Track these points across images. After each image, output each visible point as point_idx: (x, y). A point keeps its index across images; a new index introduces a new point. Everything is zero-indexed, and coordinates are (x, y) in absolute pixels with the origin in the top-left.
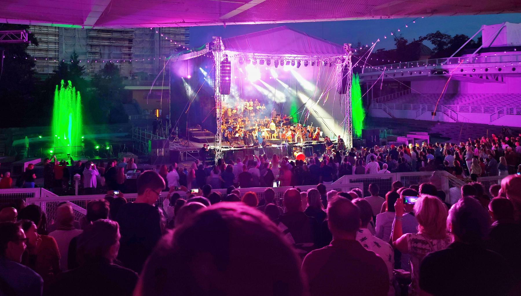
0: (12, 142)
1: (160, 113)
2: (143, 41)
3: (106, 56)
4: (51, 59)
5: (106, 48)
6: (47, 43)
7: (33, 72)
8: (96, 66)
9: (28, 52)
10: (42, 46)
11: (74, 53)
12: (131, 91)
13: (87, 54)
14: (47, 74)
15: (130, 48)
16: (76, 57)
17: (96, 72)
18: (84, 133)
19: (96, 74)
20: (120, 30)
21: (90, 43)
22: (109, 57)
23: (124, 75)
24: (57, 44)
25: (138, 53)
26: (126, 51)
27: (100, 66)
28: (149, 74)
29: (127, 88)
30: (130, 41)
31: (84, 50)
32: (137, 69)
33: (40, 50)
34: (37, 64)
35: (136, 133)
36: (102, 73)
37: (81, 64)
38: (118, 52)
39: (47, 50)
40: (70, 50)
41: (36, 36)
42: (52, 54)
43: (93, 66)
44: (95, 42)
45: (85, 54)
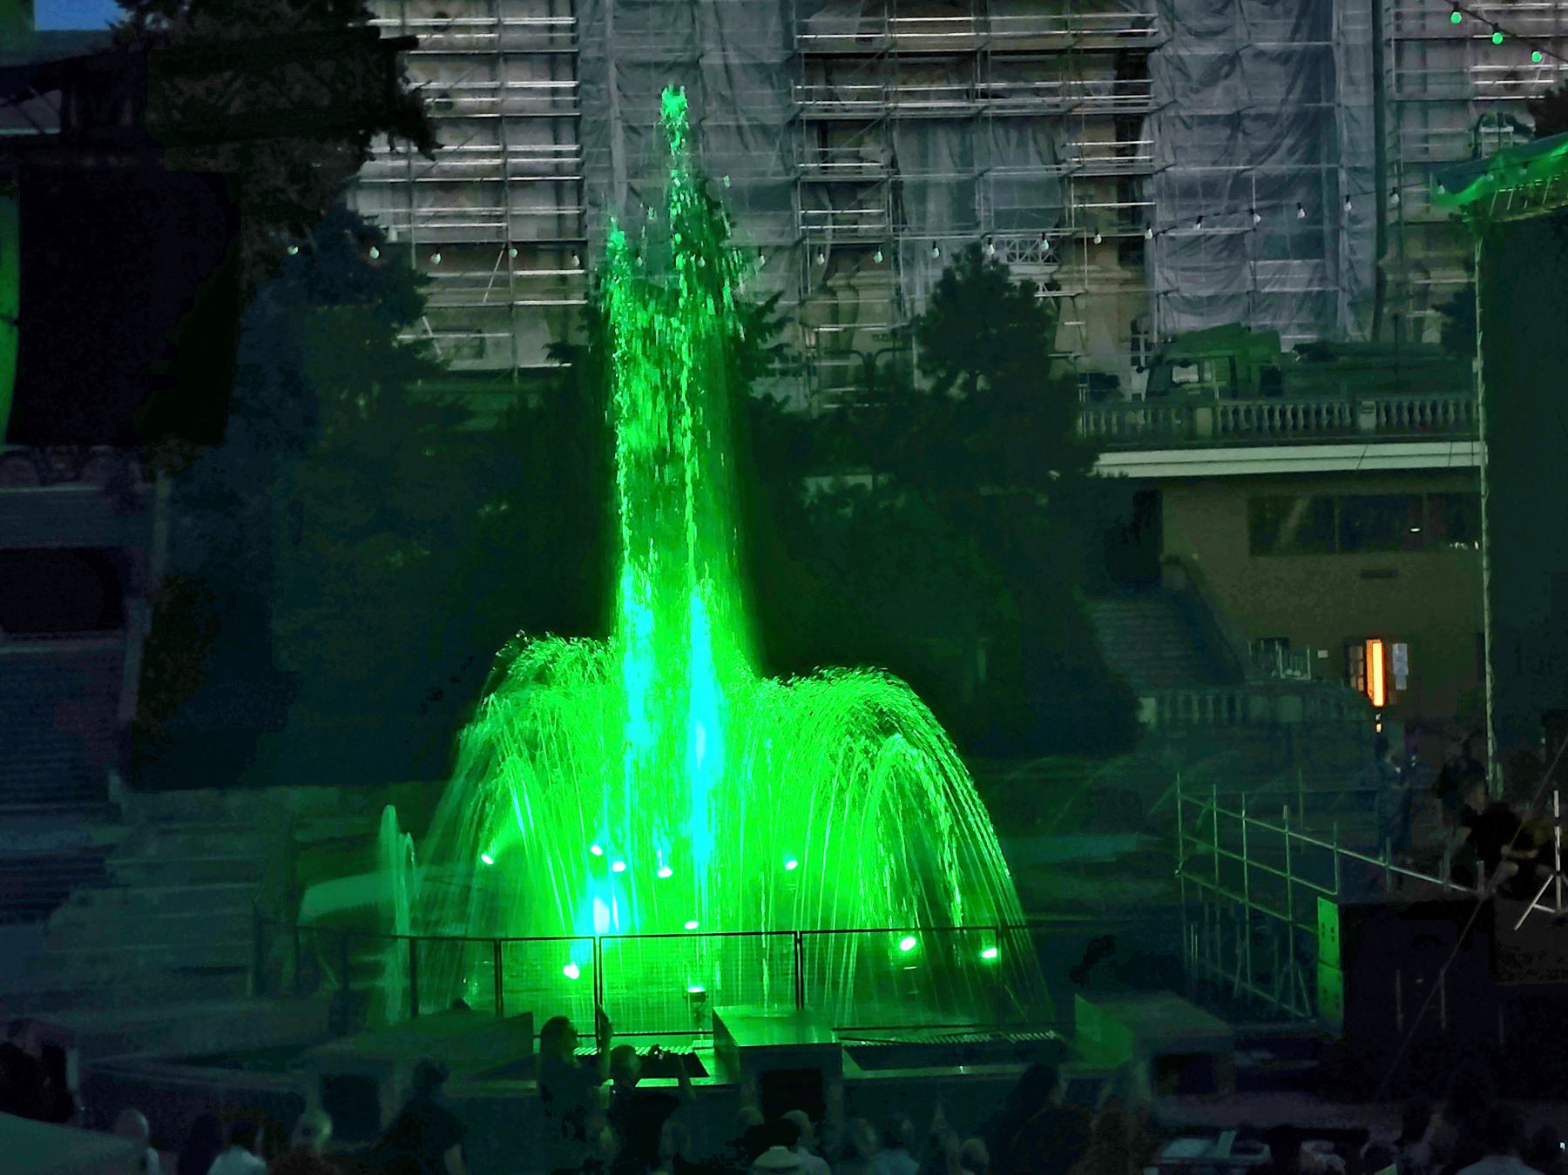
0: (295, 895)
1: (1401, 668)
2: (1233, 60)
5: (944, 144)
6: (494, 126)
7: (414, 362)
8: (865, 298)
9: (365, 206)
10: (464, 154)
12: (1149, 493)
13: (796, 198)
14: (505, 375)
15: (1127, 126)
19: (869, 361)
20: (1012, 48)
21: (816, 108)
22: (963, 213)
23: (1085, 364)
24: (567, 131)
25: (1195, 170)
26: (1095, 153)
28: (1289, 340)
29: (1110, 463)
30: (1131, 65)
31: (768, 164)
32: (1193, 305)
33: (450, 187)
34: (438, 299)
35: (1204, 834)
38: (1038, 171)
39: (498, 188)
41: (417, 79)
43: (845, 299)
44: (853, 99)
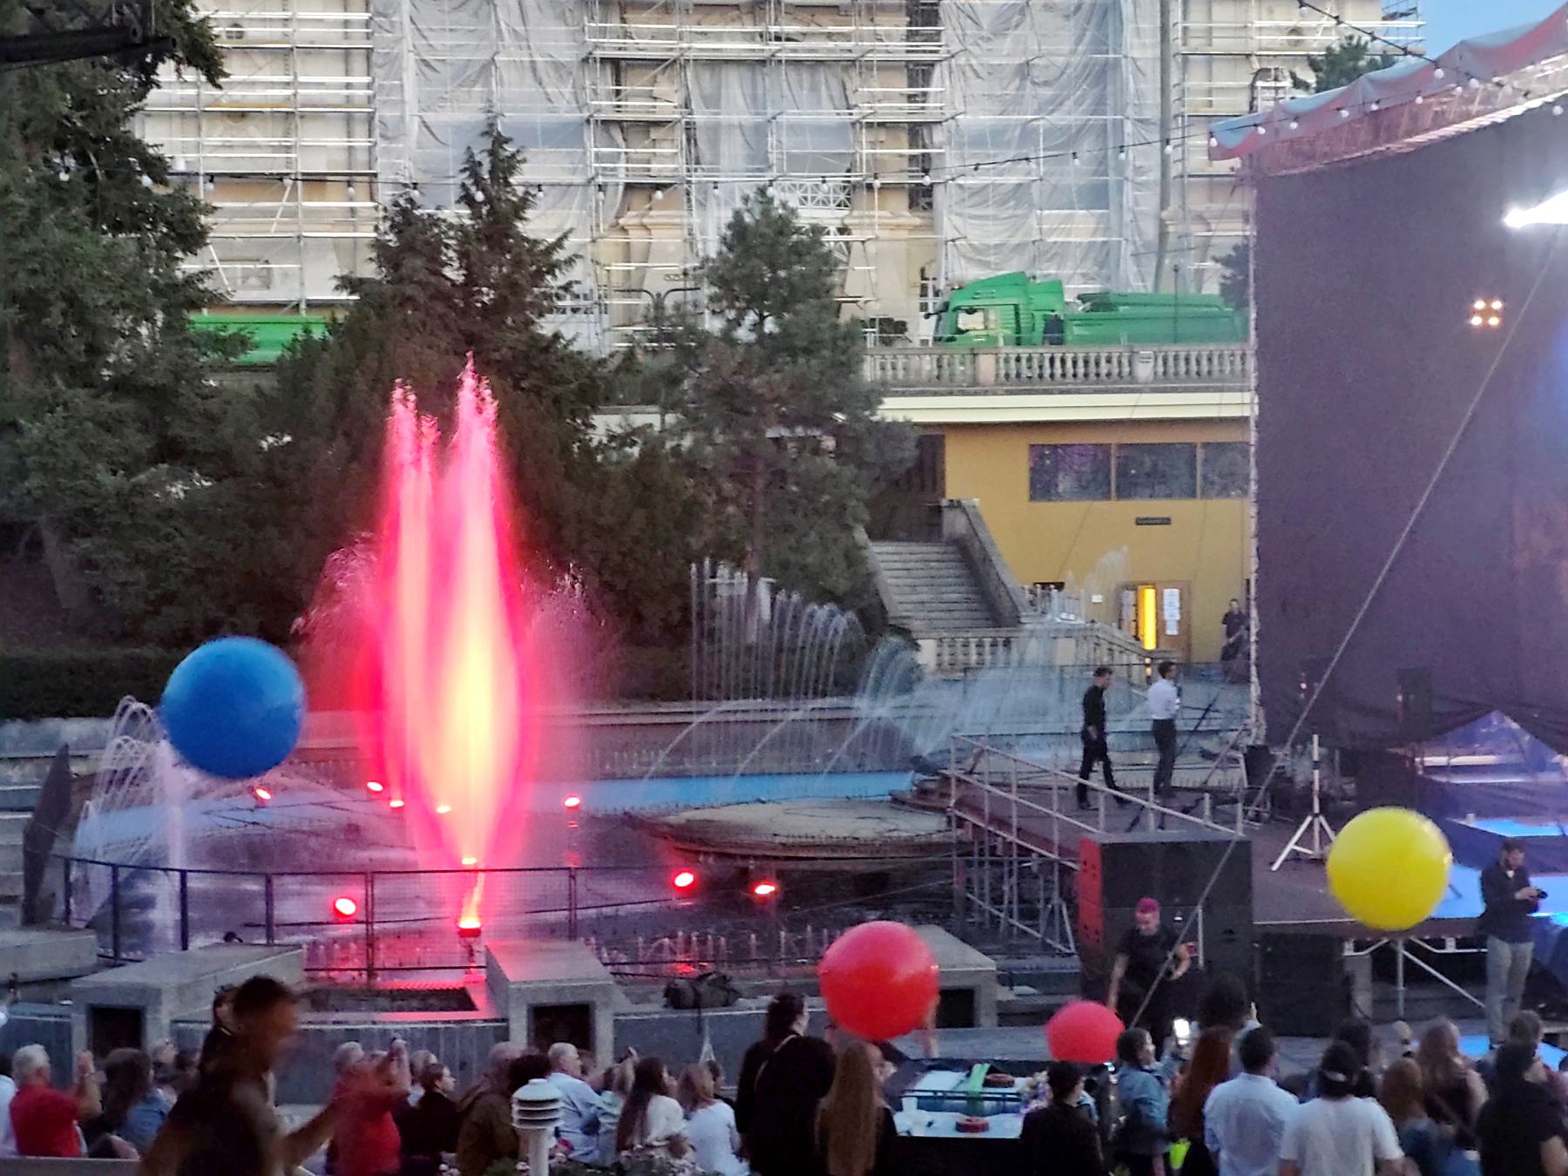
3: (733, 151)
4: (315, 181)
7: (189, 295)
10: (247, 82)
11: (489, 130)
12: (932, 439)
15: (919, 73)
16: (503, 167)
17: (655, 283)
18: (529, 1044)
21: (610, 47)
23: (875, 310)
27: (690, 241)
29: (893, 409)
36: (708, 290)
37: (537, 225)
38: (830, 115)
39: (287, 118)
40: (466, 113)
42: (322, 148)
45: (566, 136)
